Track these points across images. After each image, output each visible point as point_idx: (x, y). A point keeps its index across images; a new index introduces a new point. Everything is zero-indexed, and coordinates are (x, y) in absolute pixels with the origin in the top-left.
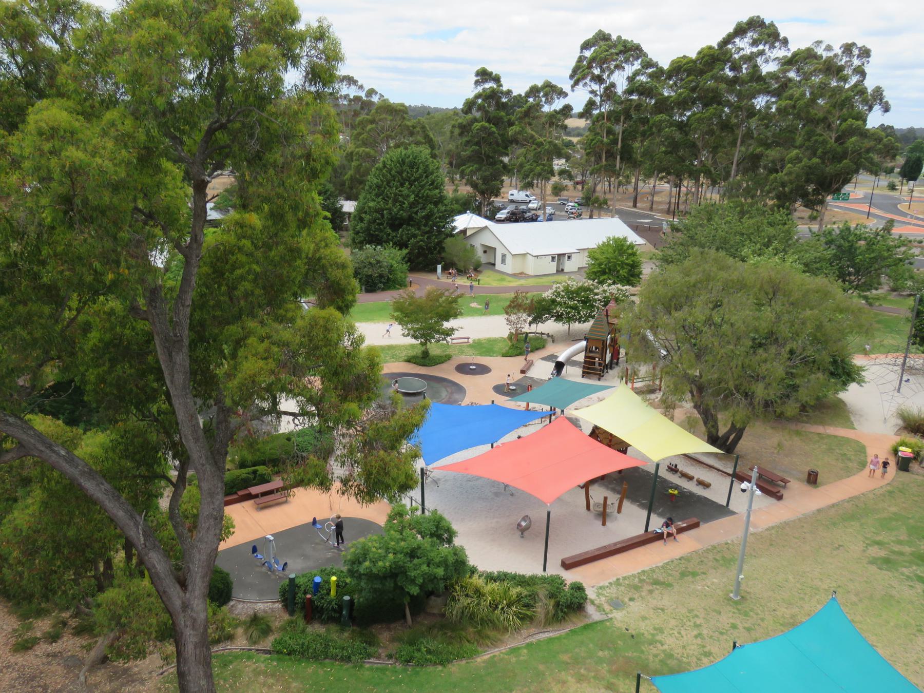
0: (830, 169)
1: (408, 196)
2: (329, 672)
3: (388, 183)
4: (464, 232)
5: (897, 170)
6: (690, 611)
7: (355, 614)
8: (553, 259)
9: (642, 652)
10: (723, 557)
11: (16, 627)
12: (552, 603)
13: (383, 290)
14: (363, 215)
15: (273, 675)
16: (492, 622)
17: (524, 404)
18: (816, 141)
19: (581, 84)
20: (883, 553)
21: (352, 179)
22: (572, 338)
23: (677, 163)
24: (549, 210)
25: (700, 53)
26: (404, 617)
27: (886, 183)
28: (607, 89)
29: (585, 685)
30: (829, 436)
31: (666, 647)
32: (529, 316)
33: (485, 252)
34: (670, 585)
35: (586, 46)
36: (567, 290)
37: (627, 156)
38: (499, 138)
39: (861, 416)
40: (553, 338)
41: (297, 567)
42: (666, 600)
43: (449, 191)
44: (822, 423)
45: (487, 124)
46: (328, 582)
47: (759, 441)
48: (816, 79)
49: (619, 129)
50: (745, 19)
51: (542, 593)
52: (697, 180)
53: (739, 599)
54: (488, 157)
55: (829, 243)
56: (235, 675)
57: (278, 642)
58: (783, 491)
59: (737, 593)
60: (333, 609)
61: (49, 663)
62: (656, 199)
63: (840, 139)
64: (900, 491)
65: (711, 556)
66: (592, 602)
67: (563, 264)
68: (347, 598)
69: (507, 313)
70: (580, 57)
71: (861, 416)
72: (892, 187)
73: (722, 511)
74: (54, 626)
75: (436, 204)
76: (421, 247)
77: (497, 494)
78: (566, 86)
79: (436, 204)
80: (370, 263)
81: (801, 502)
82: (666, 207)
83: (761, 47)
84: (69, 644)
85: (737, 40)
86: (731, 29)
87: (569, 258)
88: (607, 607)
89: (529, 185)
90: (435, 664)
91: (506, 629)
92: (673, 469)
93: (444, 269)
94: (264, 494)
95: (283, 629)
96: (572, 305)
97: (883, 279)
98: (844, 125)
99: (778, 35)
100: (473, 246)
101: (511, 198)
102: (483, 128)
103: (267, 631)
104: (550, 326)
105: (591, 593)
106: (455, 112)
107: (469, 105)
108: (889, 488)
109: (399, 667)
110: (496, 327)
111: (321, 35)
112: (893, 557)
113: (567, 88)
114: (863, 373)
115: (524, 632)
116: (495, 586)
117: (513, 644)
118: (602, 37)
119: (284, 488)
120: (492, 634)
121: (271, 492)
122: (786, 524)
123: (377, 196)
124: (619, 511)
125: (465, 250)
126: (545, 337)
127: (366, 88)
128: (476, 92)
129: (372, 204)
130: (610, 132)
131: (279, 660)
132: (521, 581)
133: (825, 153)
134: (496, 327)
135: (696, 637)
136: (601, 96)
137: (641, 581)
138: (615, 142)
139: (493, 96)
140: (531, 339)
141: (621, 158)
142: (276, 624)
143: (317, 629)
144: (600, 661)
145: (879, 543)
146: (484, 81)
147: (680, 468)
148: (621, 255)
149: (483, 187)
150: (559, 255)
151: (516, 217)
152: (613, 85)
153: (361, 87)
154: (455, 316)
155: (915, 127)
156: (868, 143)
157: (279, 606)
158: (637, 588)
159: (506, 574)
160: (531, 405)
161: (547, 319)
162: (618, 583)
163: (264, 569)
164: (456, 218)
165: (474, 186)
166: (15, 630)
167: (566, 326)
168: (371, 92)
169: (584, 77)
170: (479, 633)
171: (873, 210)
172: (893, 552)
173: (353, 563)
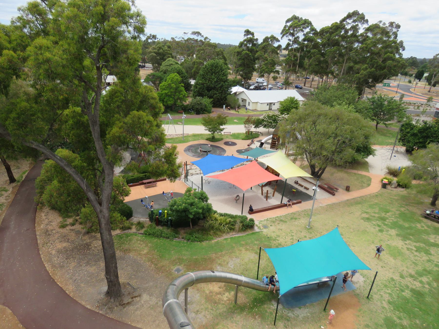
0: (378, 73)
1: (214, 79)
2: (162, 241)
3: (207, 73)
4: (235, 93)
5: (414, 75)
6: (291, 231)
7: (172, 223)
8: (268, 104)
9: (271, 243)
10: (309, 214)
11: (61, 220)
12: (242, 224)
13: (202, 114)
14: (197, 86)
15: (143, 241)
16: (220, 229)
17: (246, 157)
18: (374, 62)
19: (285, 36)
20: (367, 216)
21: (194, 72)
22: (268, 134)
23: (321, 69)
24: (270, 86)
25: (332, 25)
26: (190, 226)
27: (408, 80)
28: (295, 38)
29: (248, 252)
30: (359, 174)
31: (279, 242)
32: (254, 125)
33: (243, 101)
34: (286, 222)
35: (288, 21)
36: (269, 116)
37: (301, 66)
38: (253, 58)
39: (373, 168)
40: (262, 134)
41: (157, 207)
42: (283, 226)
43: (231, 77)
44: (355, 169)
45: (248, 52)
46: (164, 213)
47: (331, 174)
48: (379, 36)
49: (298, 55)
50: (351, 11)
51: (238, 221)
52: (328, 76)
53: (310, 228)
54: (247, 65)
55: (373, 102)
56: (130, 240)
57: (146, 231)
58: (335, 193)
59: (309, 226)
60: (165, 222)
61: (70, 232)
62: (313, 83)
63: (384, 61)
64: (380, 195)
65: (303, 214)
66: (257, 226)
67: (272, 106)
68: (170, 218)
69: (245, 124)
70: (285, 26)
71: (373, 168)
72: (410, 82)
73: (308, 197)
74: (73, 221)
75: (224, 82)
76: (218, 99)
77: (230, 188)
78: (279, 37)
79: (224, 82)
80: (198, 104)
81: (342, 196)
82: (316, 86)
83: (357, 23)
84: (78, 227)
85: (348, 20)
86: (345, 15)
87: (274, 104)
88: (262, 228)
89: (262, 76)
90: (198, 241)
91: (224, 232)
92: (296, 183)
93: (226, 107)
94: (148, 183)
95: (148, 227)
96: (271, 121)
97: (395, 117)
98: (386, 56)
99: (364, 18)
100: (238, 99)
101: (257, 81)
102: (246, 54)
103: (143, 227)
104: (261, 129)
105: (256, 222)
106: (236, 47)
107: (241, 44)
108: (377, 194)
109: (185, 241)
110: (241, 129)
111: (138, 15)
112: (371, 217)
113: (279, 39)
114: (375, 152)
115: (231, 234)
116: (222, 217)
117: (226, 237)
118: (295, 18)
119: (154, 182)
120: (219, 233)
121: (150, 182)
122: (334, 204)
123: (203, 78)
124: (273, 196)
125: (235, 100)
126: (259, 133)
127: (205, 36)
128: (244, 39)
129: (200, 82)
130: (295, 56)
131: (145, 237)
132: (232, 216)
133: (377, 66)
134: (241, 129)
135: (291, 239)
136: (293, 42)
137: (276, 220)
138: (297, 60)
139: (250, 41)
140: (254, 134)
141: (299, 67)
142: (146, 225)
143: (160, 228)
144: (255, 244)
145: (367, 213)
146: (247, 35)
147: (299, 182)
148: (292, 104)
149: (245, 76)
150: (270, 103)
151: (258, 88)
152: (298, 37)
153: (203, 36)
154: (225, 124)
155: (427, 58)
156: (395, 63)
157: (148, 220)
158: (274, 222)
159: (227, 214)
160: (249, 157)
161: (260, 127)
162: (267, 220)
163: (145, 208)
164: (232, 88)
165: (242, 76)
166: (61, 221)
167: (267, 130)
168: (206, 38)
169: (287, 33)
170: (215, 233)
171: (398, 91)
172: (371, 216)
173: (172, 206)
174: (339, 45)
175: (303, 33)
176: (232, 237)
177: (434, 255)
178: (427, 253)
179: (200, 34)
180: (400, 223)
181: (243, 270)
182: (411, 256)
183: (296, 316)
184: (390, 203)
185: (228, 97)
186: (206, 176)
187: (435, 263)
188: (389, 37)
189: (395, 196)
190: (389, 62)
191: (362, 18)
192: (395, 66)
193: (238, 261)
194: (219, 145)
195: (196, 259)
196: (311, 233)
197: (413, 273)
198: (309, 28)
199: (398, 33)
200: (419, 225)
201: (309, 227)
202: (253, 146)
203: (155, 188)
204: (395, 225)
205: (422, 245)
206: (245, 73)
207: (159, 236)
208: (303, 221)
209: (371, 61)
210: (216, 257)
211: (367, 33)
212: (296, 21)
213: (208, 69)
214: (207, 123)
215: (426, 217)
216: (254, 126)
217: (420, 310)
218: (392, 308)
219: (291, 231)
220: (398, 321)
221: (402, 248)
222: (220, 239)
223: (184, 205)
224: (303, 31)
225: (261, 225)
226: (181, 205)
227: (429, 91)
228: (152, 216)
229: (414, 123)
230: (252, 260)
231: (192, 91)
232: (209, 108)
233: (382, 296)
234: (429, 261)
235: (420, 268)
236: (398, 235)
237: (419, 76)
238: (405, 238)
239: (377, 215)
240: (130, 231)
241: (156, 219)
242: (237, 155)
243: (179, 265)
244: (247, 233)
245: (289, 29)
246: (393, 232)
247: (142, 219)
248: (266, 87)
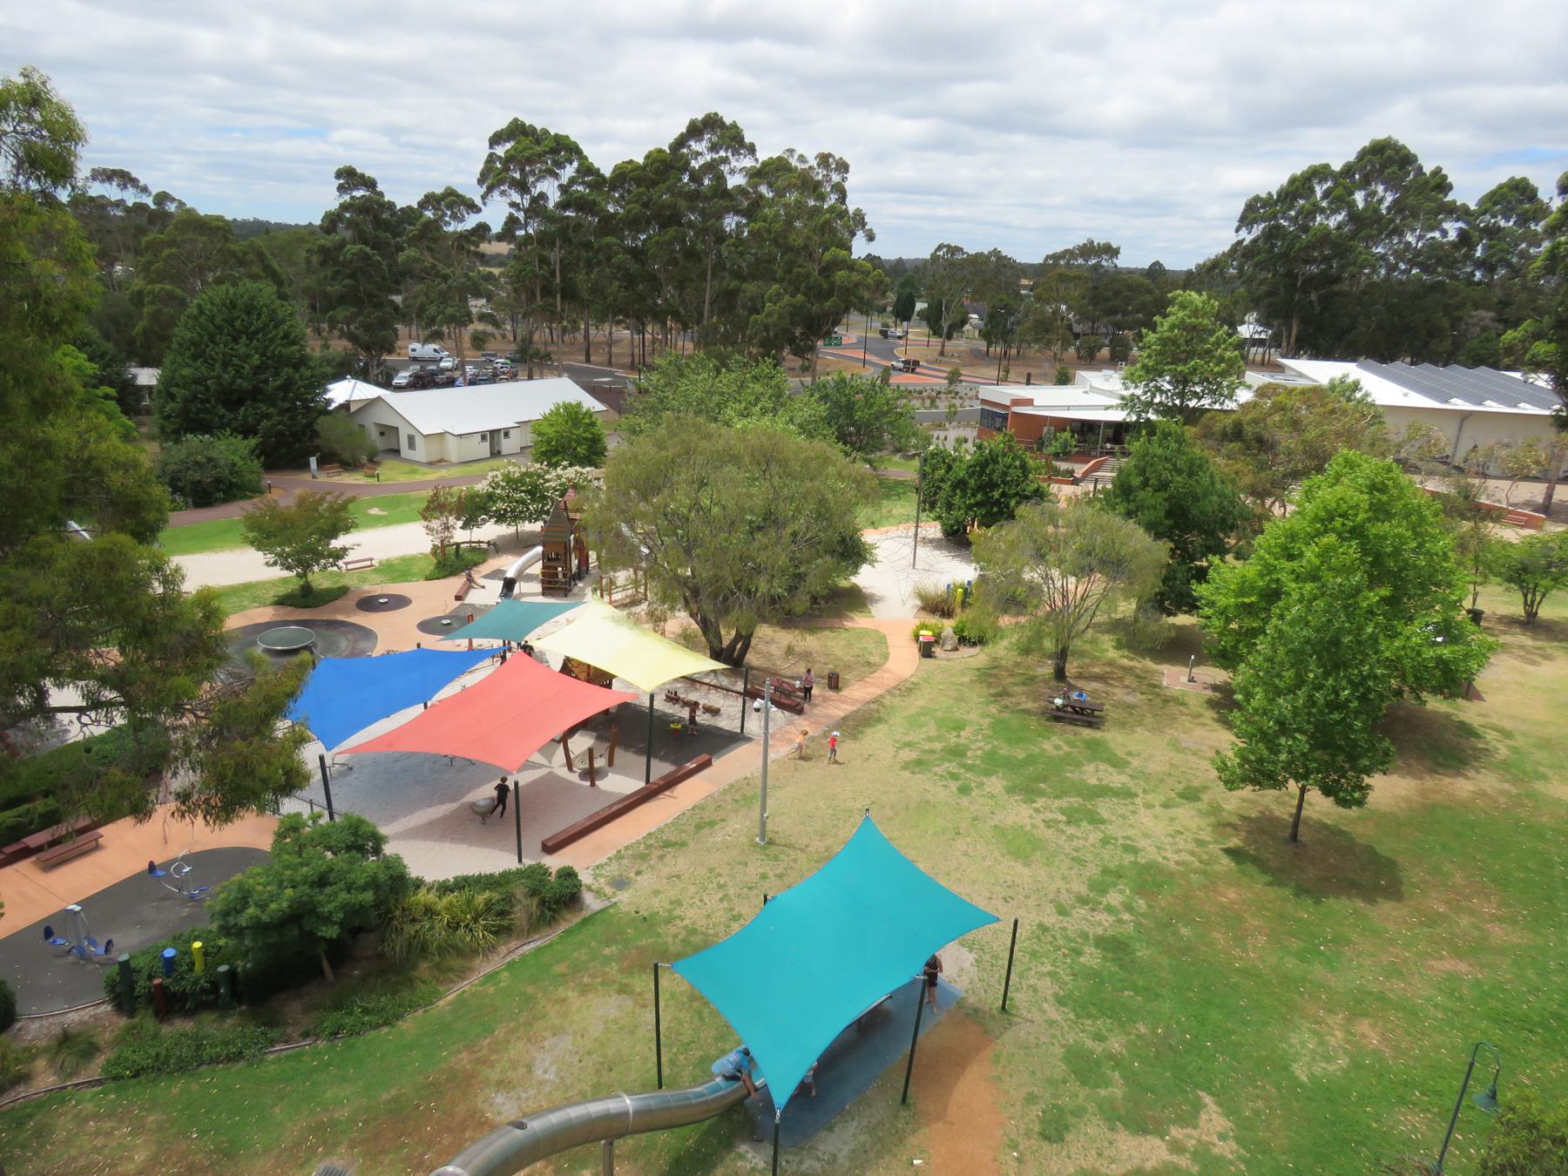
1: (248, 357)
2: (210, 1082)
3: (212, 338)
4: (345, 406)
5: (889, 309)
6: (711, 870)
8: (484, 438)
9: (659, 935)
12: (535, 901)
14: (174, 390)
17: (464, 643)
19: (496, 194)
20: (914, 755)
22: (519, 544)
25: (647, 157)
26: (321, 973)
28: (534, 200)
29: (591, 996)
32: (458, 519)
33: (382, 434)
34: (683, 844)
35: (496, 140)
42: (680, 863)
43: (314, 348)
46: (188, 952)
48: (792, 197)
51: (519, 891)
56: (41, 1133)
59: (763, 835)
60: (203, 990)
65: (729, 798)
66: (589, 888)
67: (499, 443)
69: (425, 519)
70: (491, 155)
75: (296, 366)
76: (280, 434)
78: (475, 193)
79: (296, 366)
80: (196, 463)
83: (722, 153)
87: (506, 435)
88: (608, 890)
90: (378, 1026)
91: (475, 952)
93: (320, 463)
94: (53, 844)
96: (521, 498)
98: (827, 256)
100: (362, 426)
101: (413, 354)
104: (490, 531)
105: (585, 877)
107: (332, 221)
112: (925, 757)
115: (503, 949)
116: (450, 897)
118: (517, 130)
123: (195, 358)
129: (186, 372)
130: (543, 261)
135: (721, 900)
136: (526, 211)
137: (648, 847)
138: (553, 274)
145: (908, 744)
150: (492, 432)
151: (425, 380)
153: (145, 190)
154: (347, 530)
156: (855, 277)
158: (643, 857)
162: (619, 856)
164: (330, 387)
165: (353, 338)
167: (512, 530)
168: (162, 198)
169: (501, 182)
170: (438, 967)
172: (925, 751)
174: (680, 224)
175: (556, 183)
176: (513, 963)
177: (1111, 822)
178: (1096, 820)
179: (134, 182)
180: (1002, 752)
181: (598, 1072)
182: (1061, 842)
183: (828, 1162)
184: (957, 700)
185: (322, 423)
186: (336, 750)
187: (1121, 841)
188: (822, 198)
189: (964, 675)
190: (840, 275)
191: (733, 139)
192: (857, 285)
193: (567, 1043)
194: (340, 618)
195: (395, 1100)
196: (776, 859)
197: (1084, 890)
198: (575, 164)
199: (847, 185)
200: (1047, 746)
201: (762, 839)
202: (474, 598)
203: (97, 857)
204: (992, 763)
205: (1075, 801)
206: (367, 328)
207: (161, 1067)
208: (740, 826)
209: (789, 271)
210: (478, 1061)
211: (755, 187)
212: (526, 142)
213: (212, 319)
214: (269, 535)
215: (1057, 719)
216: (460, 523)
217: (1136, 992)
218: (1072, 1016)
219: (711, 870)
220: (1098, 1048)
221: (1033, 826)
222: (465, 986)
223: (289, 892)
224: (556, 176)
225: (602, 880)
226: (273, 898)
227: (942, 354)
228: (126, 991)
229: (50, 417)
230: (615, 1021)
231: (148, 412)
232: (249, 476)
233: (1036, 991)
234: (1105, 841)
235: (1093, 870)
236: (1010, 790)
237: (903, 312)
238: (1028, 791)
239: (938, 746)
240: (22, 1091)
241: (149, 994)
242: (433, 642)
243: (327, 1153)
244: (563, 927)
245: (506, 169)
246: (995, 784)
247: (74, 1017)
248: (457, 374)
